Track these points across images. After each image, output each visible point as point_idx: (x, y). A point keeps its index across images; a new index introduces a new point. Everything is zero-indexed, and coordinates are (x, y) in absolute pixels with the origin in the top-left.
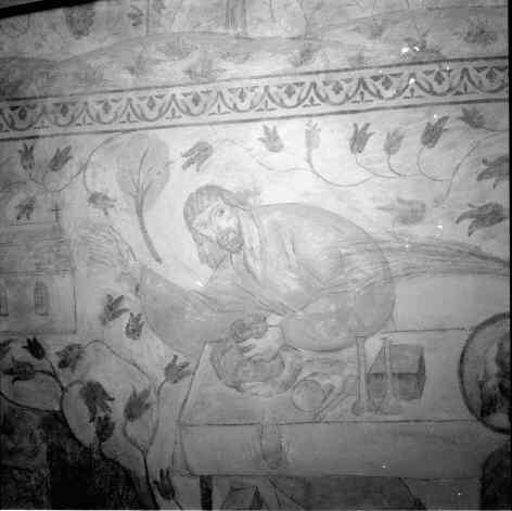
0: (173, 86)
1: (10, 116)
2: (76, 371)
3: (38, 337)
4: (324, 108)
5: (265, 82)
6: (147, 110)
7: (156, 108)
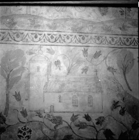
0: (134, 35)
1: (79, 38)
2: (102, 126)
3: (40, 112)
4: (64, 44)
5: (120, 36)
6: (126, 42)
7: (129, 41)
